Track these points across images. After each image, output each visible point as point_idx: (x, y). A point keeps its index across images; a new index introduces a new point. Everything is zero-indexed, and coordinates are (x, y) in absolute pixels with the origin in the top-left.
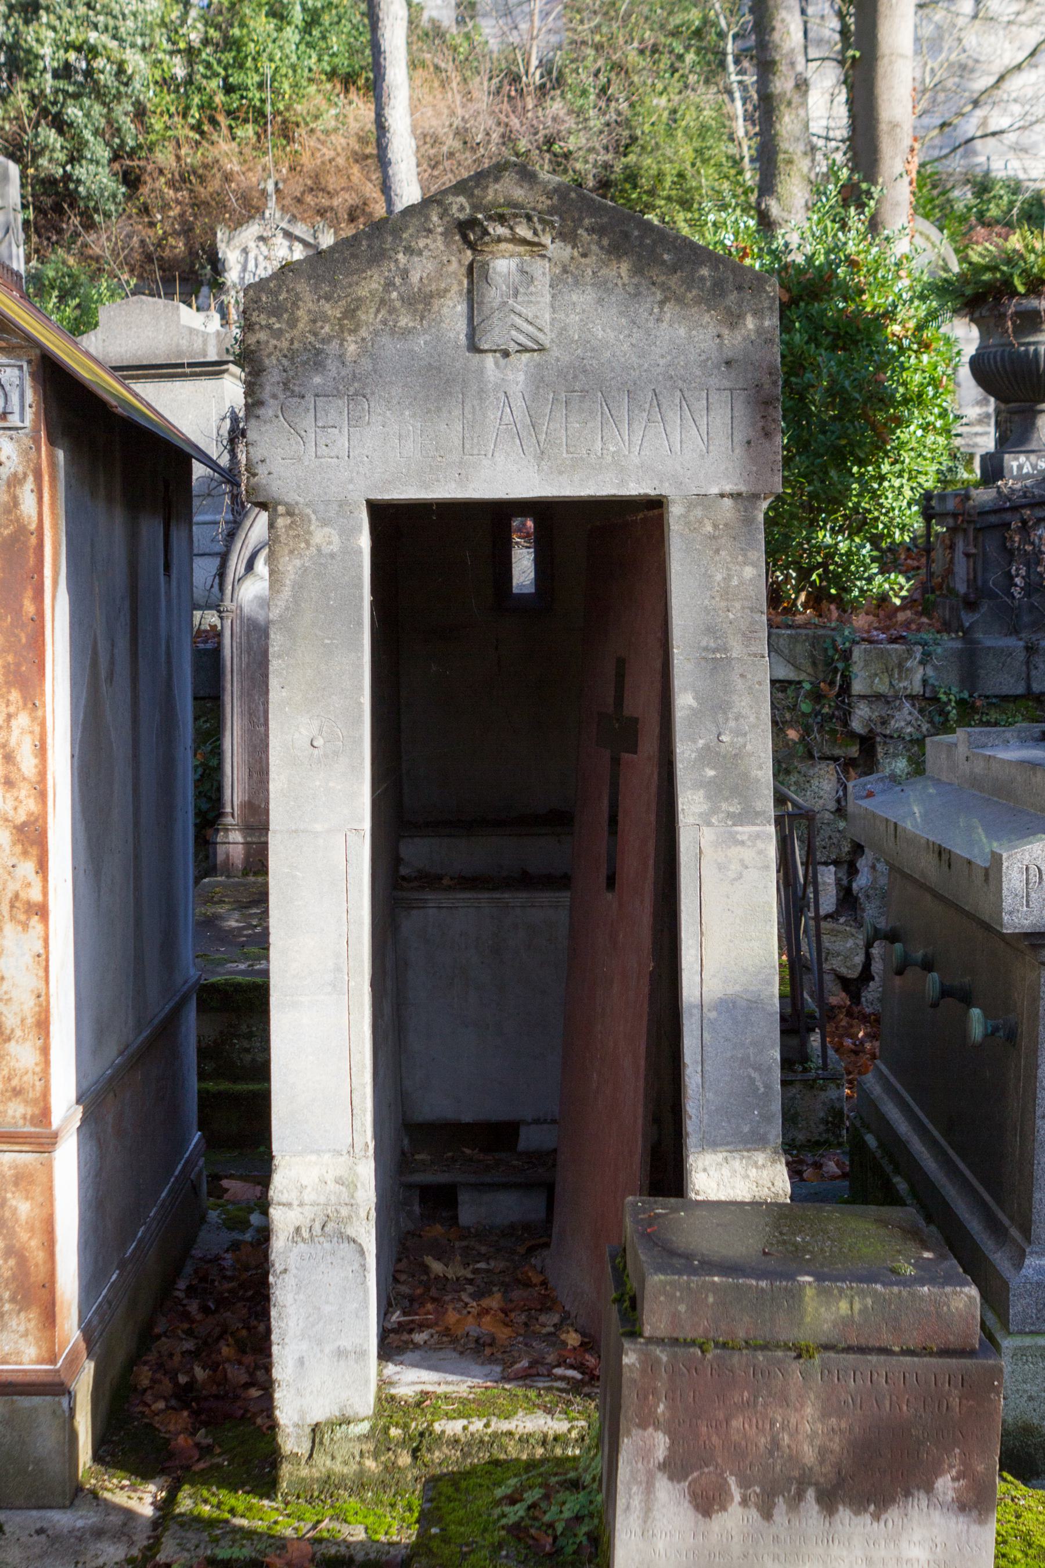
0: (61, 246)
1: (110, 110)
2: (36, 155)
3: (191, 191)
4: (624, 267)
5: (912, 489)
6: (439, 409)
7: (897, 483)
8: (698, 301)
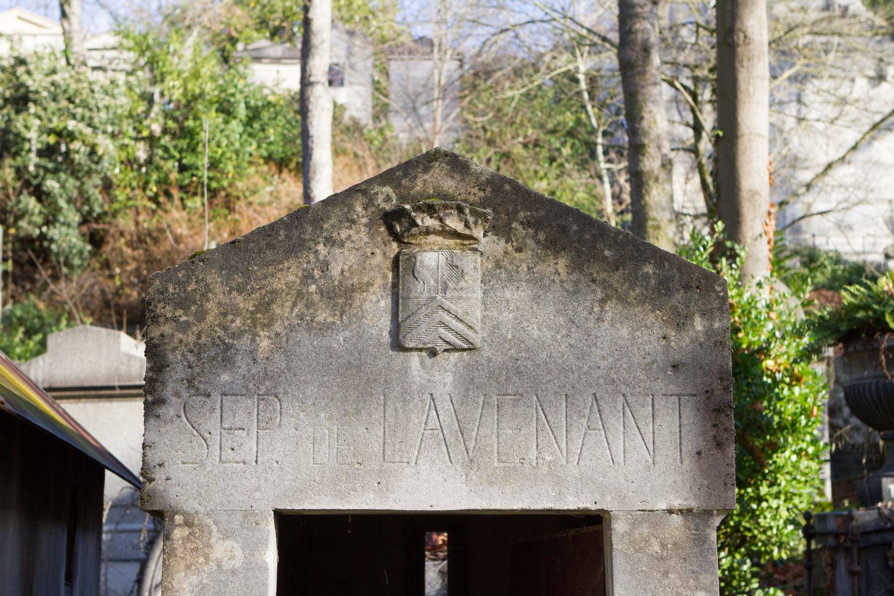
0: (34, 293)
1: (83, 183)
2: (18, 218)
3: (146, 250)
4: (562, 264)
5: (788, 510)
6: (358, 412)
7: (774, 503)
8: (642, 300)
